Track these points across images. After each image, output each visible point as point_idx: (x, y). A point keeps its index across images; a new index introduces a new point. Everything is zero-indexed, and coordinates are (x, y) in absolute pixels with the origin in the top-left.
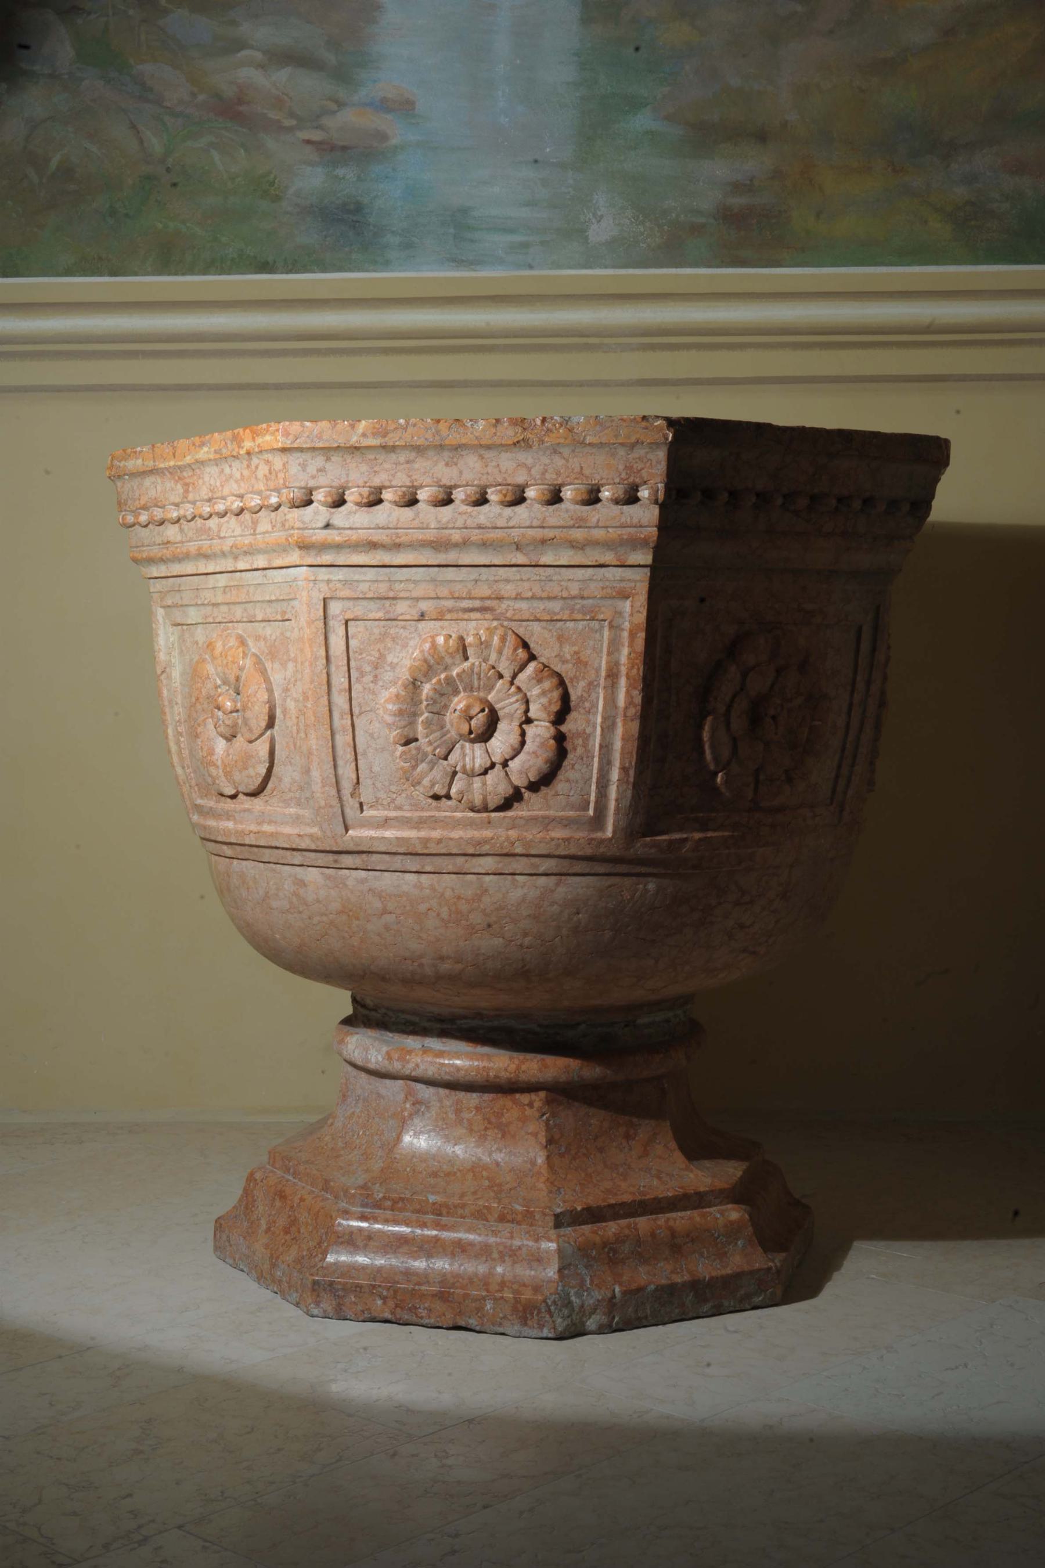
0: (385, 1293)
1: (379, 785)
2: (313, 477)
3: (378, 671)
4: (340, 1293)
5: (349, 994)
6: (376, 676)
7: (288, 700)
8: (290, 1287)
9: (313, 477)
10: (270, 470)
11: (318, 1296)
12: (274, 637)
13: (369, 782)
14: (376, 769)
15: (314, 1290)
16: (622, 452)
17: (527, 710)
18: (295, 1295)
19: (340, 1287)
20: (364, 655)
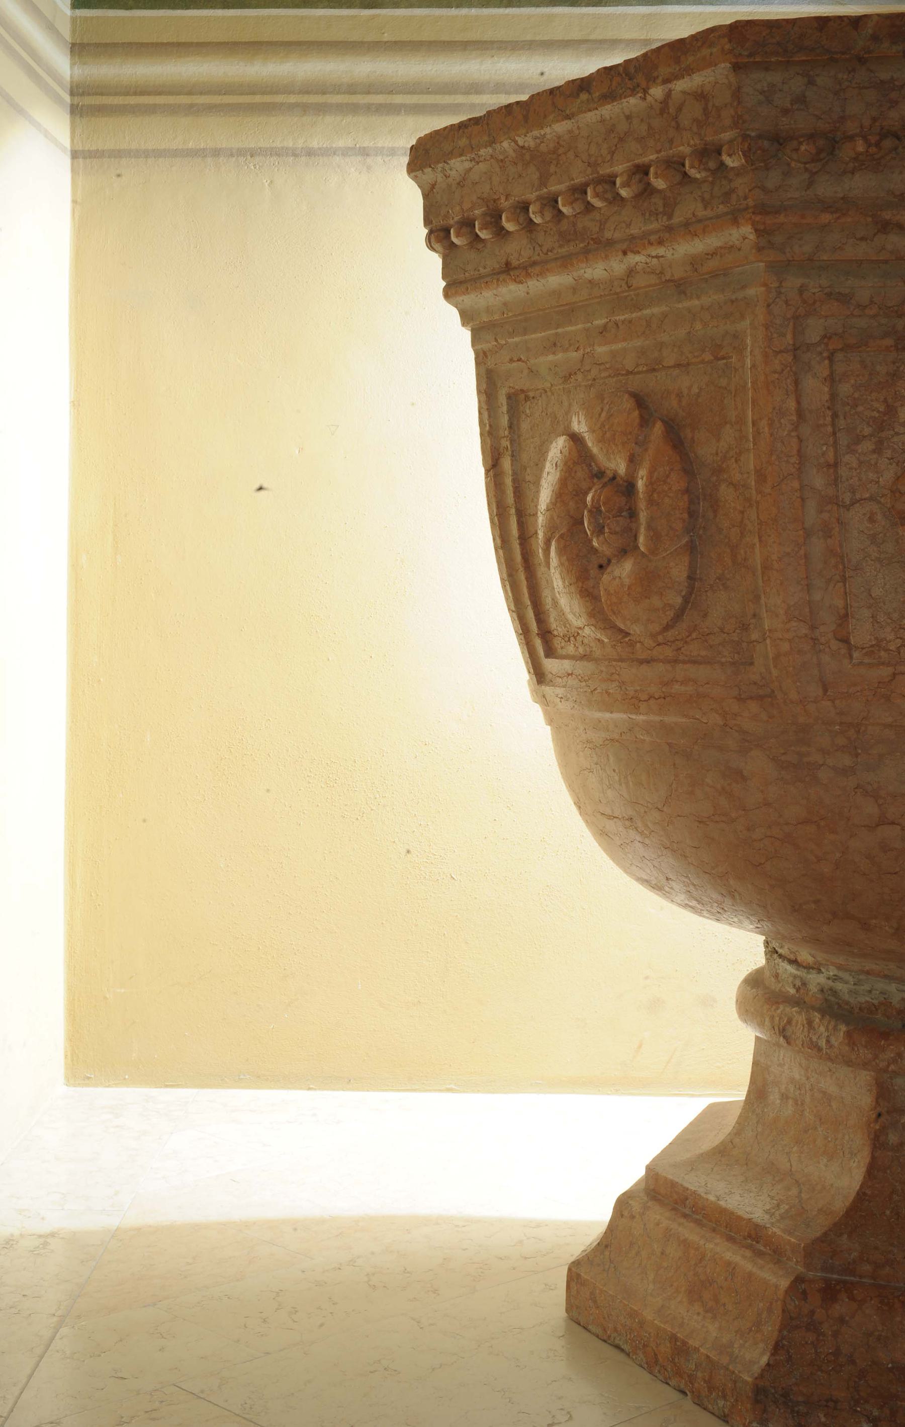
0: (876, 1413)
1: (881, 618)
2: (786, 112)
3: (883, 435)
4: (802, 1409)
5: (764, 938)
6: (880, 442)
7: (723, 487)
8: (711, 1389)
9: (786, 112)
10: (705, 109)
11: (765, 1411)
12: (695, 390)
13: (866, 613)
14: (877, 592)
15: (757, 1401)
16: (777, 300)
17: (692, 568)
18: (721, 1403)
19: (801, 1399)
20: (860, 409)
